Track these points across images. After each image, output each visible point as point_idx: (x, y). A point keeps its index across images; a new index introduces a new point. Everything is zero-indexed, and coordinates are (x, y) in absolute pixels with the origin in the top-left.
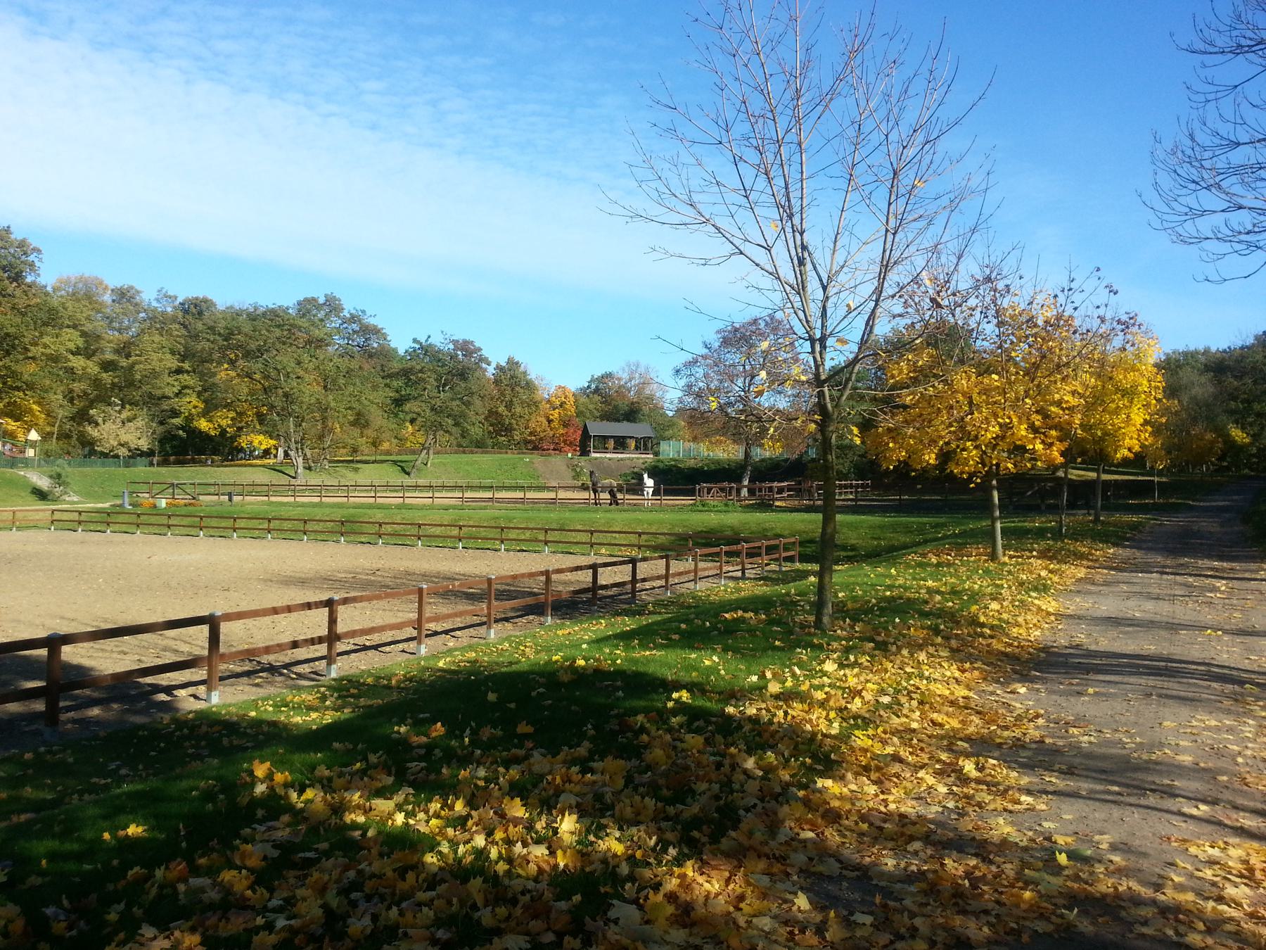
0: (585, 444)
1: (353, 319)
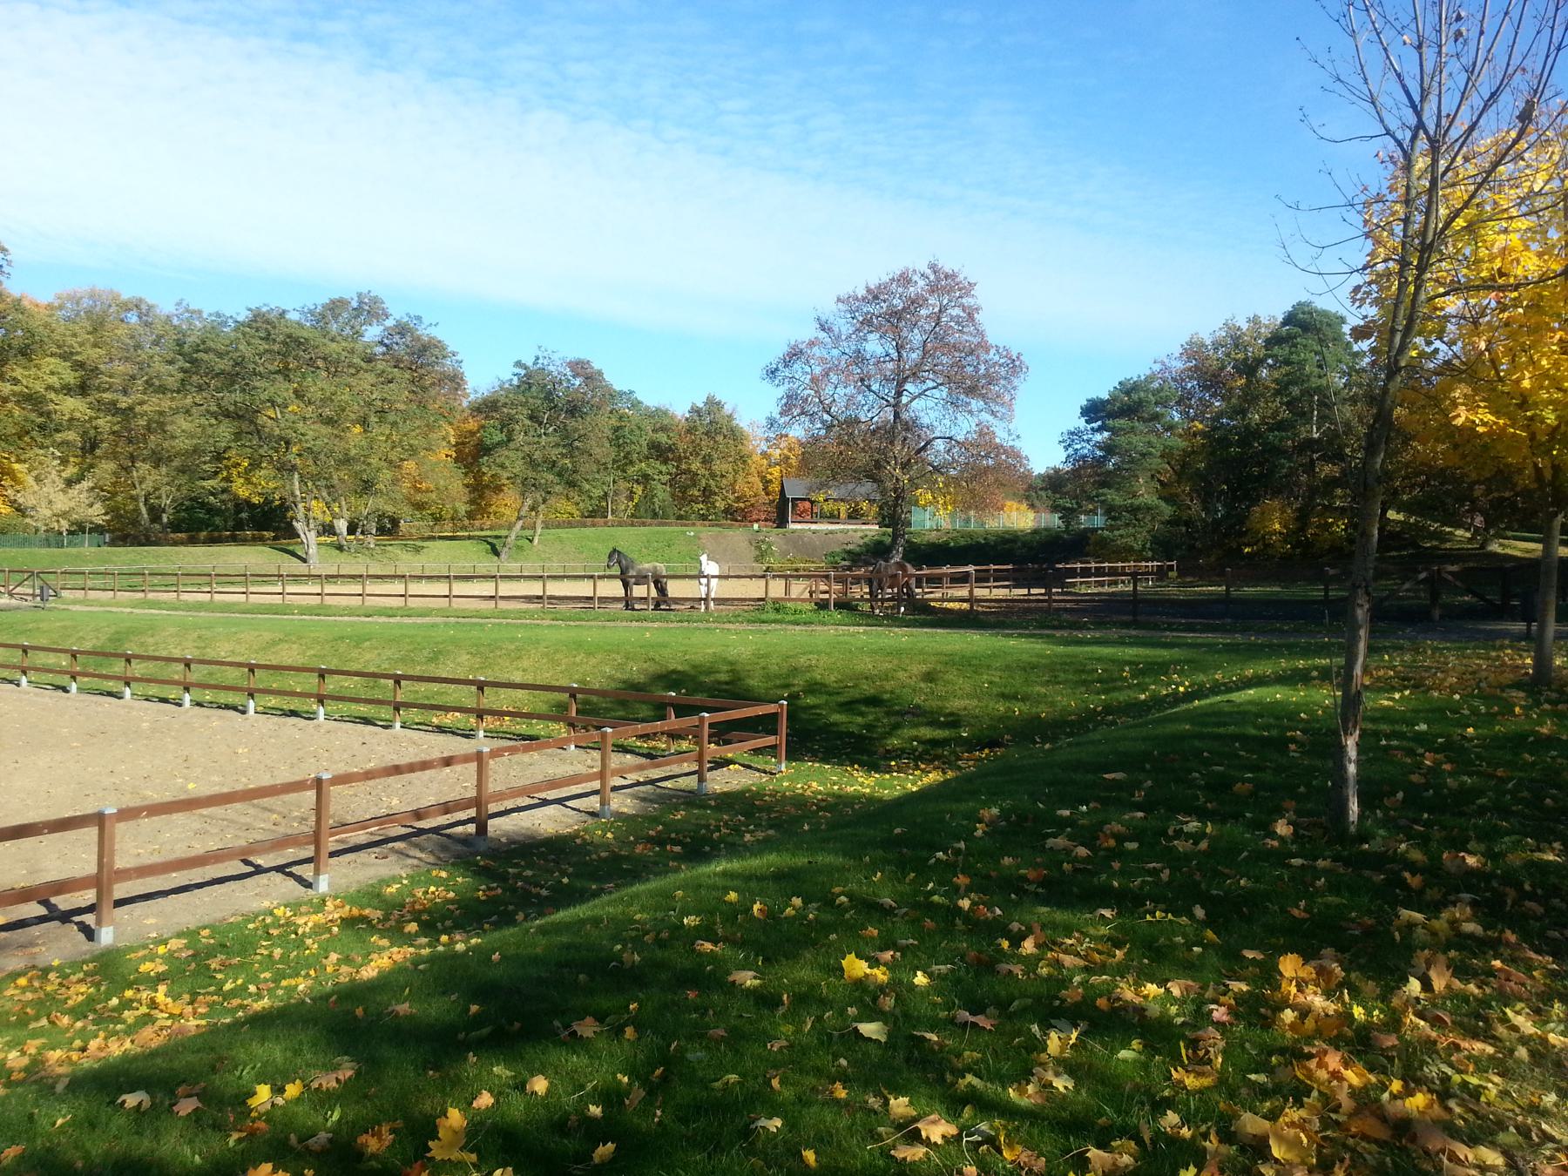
0: (781, 511)
1: (402, 330)
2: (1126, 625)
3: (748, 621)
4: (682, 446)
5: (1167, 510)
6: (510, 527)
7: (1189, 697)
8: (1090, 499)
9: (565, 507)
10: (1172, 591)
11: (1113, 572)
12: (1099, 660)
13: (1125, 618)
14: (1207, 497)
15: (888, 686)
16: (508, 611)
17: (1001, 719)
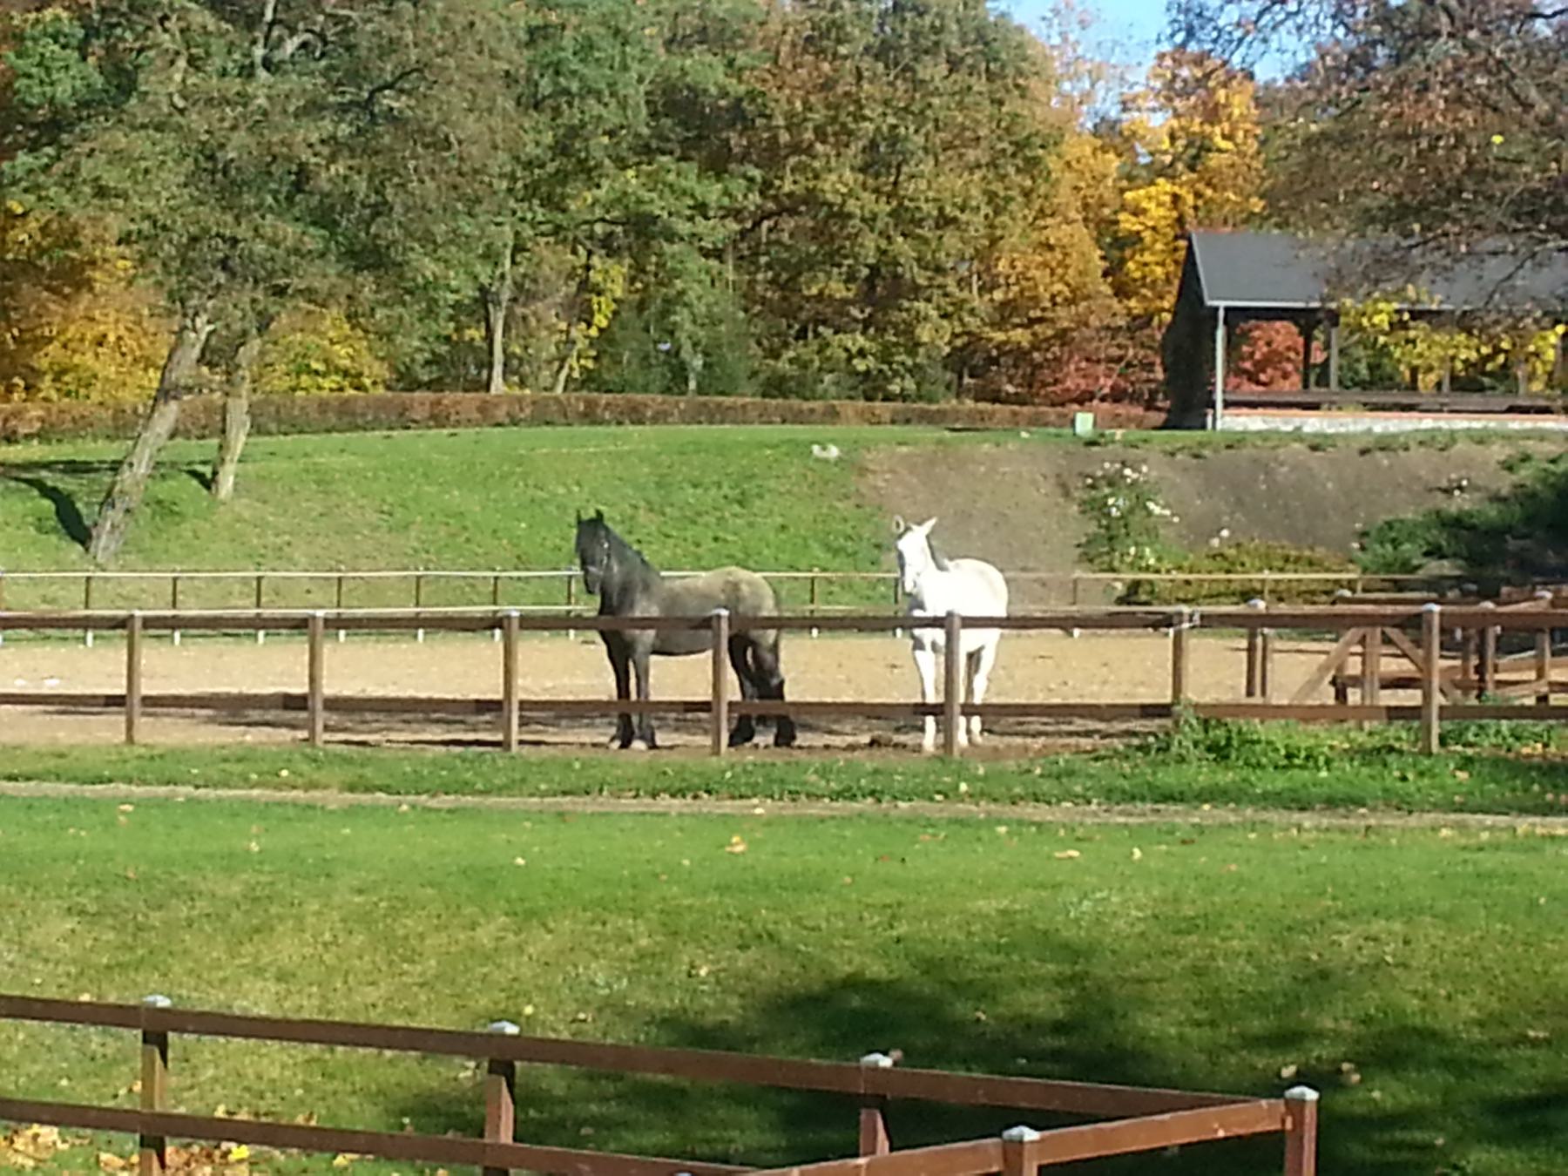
0: (1182, 364)
3: (1109, 794)
4: (781, 103)
6: (125, 425)
9: (331, 342)
16: (179, 755)
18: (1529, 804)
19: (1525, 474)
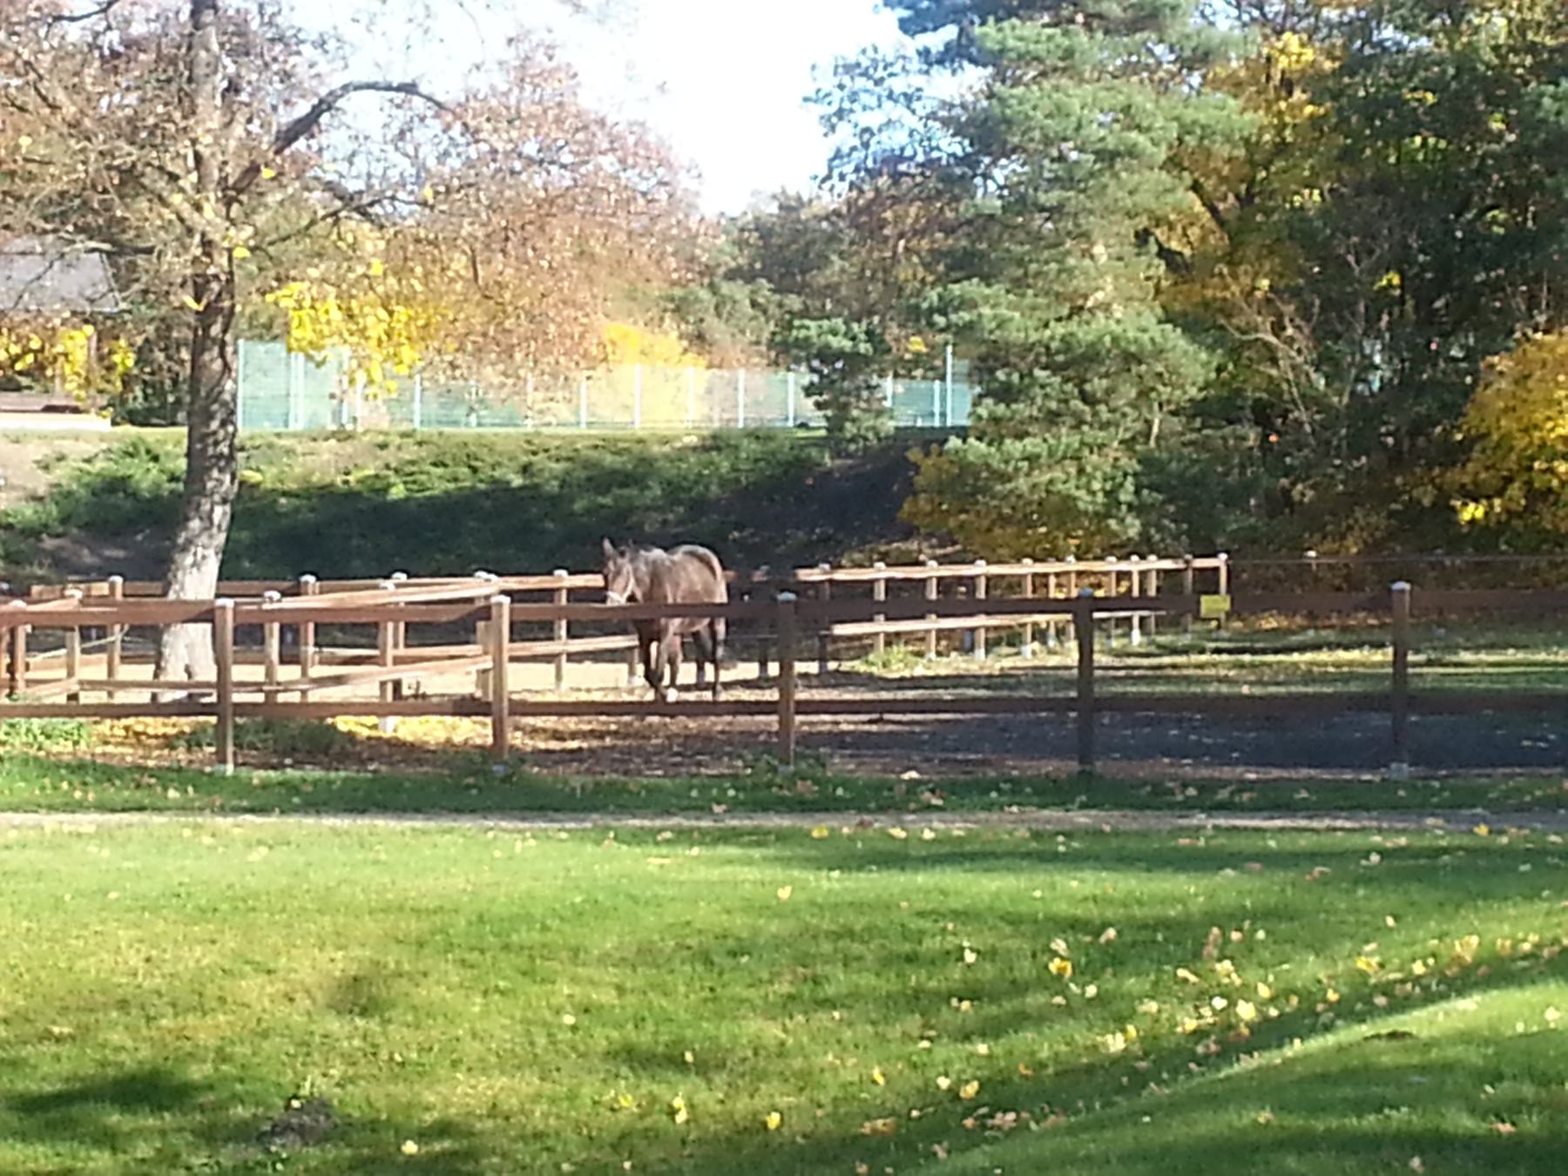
2: (1054, 793)
5: (1193, 365)
7: (1270, 1033)
8: (917, 317)
10: (1214, 668)
11: (1003, 597)
12: (962, 916)
13: (1049, 767)
14: (1332, 316)
15: (206, 1031)
17: (622, 1141)
18: (58, 801)
19: (61, 474)
